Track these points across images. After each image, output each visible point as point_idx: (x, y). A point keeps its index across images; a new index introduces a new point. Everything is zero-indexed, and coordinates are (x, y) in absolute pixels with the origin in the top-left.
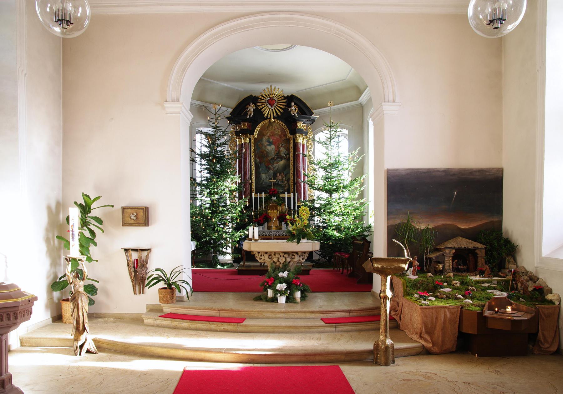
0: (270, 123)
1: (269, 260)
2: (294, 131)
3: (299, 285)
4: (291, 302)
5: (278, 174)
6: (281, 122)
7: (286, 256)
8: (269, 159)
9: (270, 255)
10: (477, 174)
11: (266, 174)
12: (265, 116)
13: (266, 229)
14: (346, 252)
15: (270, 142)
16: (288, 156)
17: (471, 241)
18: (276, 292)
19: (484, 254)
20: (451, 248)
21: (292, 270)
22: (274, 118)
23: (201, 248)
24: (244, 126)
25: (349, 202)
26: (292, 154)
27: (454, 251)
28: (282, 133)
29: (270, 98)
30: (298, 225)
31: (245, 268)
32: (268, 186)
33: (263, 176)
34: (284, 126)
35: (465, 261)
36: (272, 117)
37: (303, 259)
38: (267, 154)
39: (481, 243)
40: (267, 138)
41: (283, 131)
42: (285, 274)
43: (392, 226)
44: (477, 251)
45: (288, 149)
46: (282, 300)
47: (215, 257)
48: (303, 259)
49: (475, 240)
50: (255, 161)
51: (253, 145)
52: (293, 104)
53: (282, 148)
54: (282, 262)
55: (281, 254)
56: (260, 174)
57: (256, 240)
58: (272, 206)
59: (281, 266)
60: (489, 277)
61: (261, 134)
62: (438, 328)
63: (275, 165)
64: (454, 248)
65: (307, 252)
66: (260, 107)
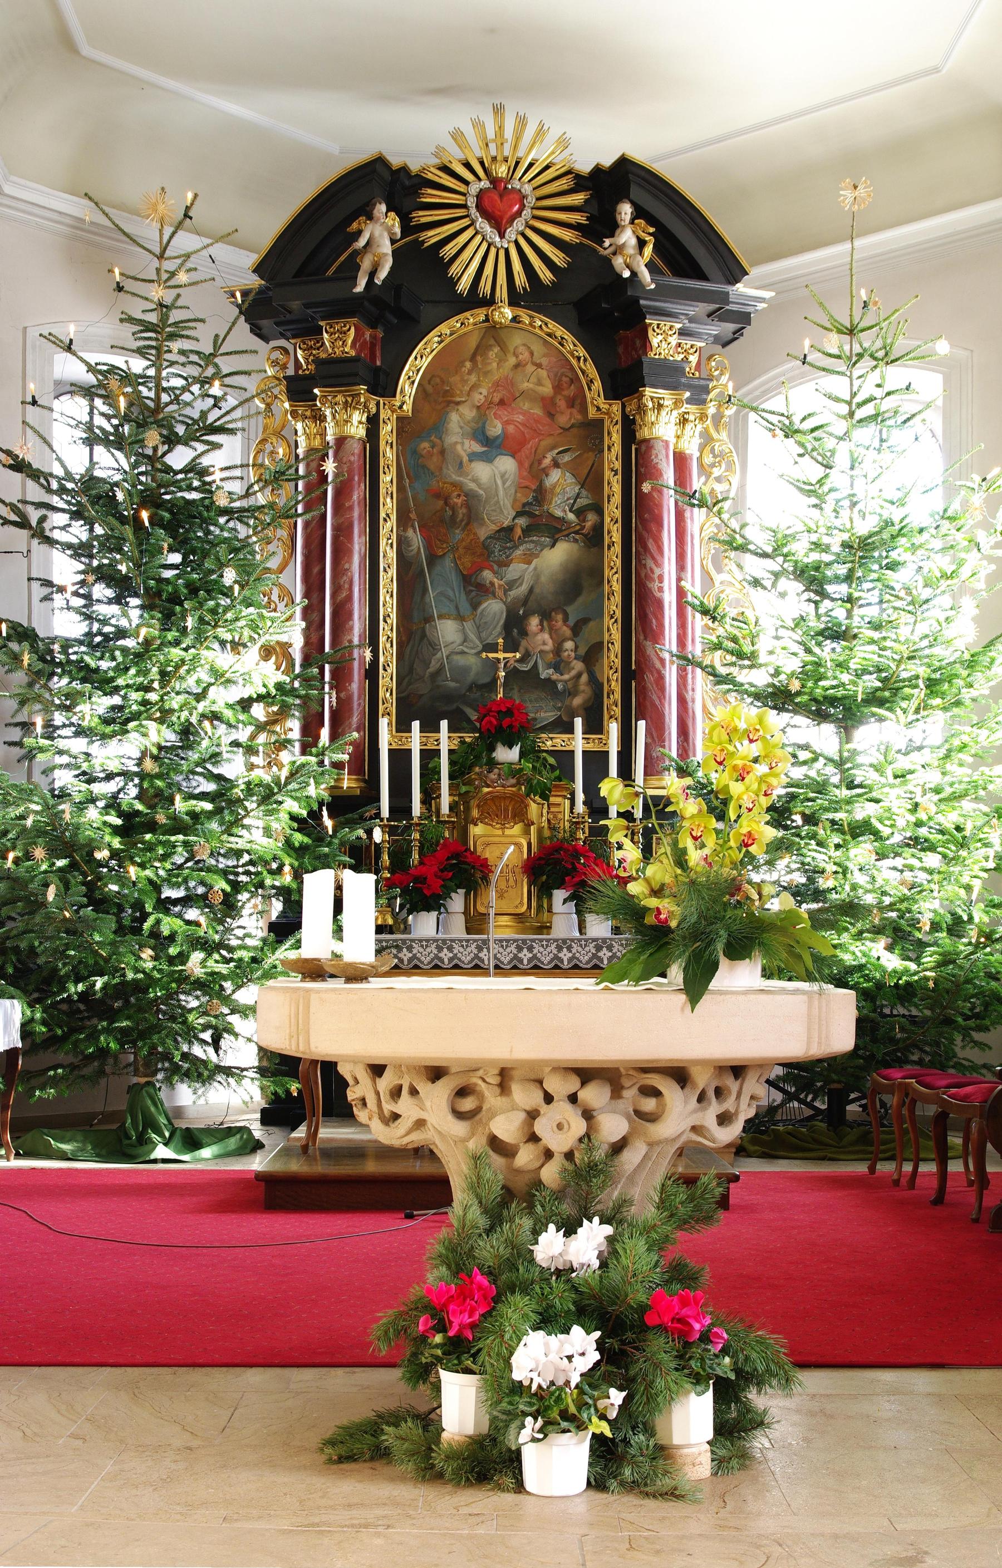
0: (492, 330)
1: (459, 1128)
2: (628, 376)
3: (706, 1337)
4: (638, 1487)
5: (534, 622)
6: (554, 327)
7: (594, 1095)
8: (483, 533)
9: (465, 1089)
11: (460, 618)
12: (464, 285)
13: (457, 928)
15: (487, 441)
16: (591, 518)
18: (510, 1399)
21: (645, 1210)
22: (515, 299)
23: (51, 1042)
24: (341, 340)
25: (960, 773)
26: (613, 509)
28: (558, 388)
29: (495, 181)
30: (694, 856)
31: (320, 1168)
32: (474, 686)
33: (448, 631)
34: (573, 347)
36: (502, 292)
37: (724, 1119)
38: (472, 507)
40: (468, 412)
41: (567, 379)
42: (585, 1246)
45: (592, 481)
46: (557, 1465)
47: (139, 1096)
48: (724, 1119)
50: (402, 544)
51: (388, 454)
52: (626, 210)
53: (555, 476)
54: (559, 1142)
55: (557, 1085)
56: (429, 619)
57: (356, 975)
58: (495, 798)
59: (551, 1174)
61: (436, 393)
63: (515, 569)
65: (762, 1065)
66: (432, 236)
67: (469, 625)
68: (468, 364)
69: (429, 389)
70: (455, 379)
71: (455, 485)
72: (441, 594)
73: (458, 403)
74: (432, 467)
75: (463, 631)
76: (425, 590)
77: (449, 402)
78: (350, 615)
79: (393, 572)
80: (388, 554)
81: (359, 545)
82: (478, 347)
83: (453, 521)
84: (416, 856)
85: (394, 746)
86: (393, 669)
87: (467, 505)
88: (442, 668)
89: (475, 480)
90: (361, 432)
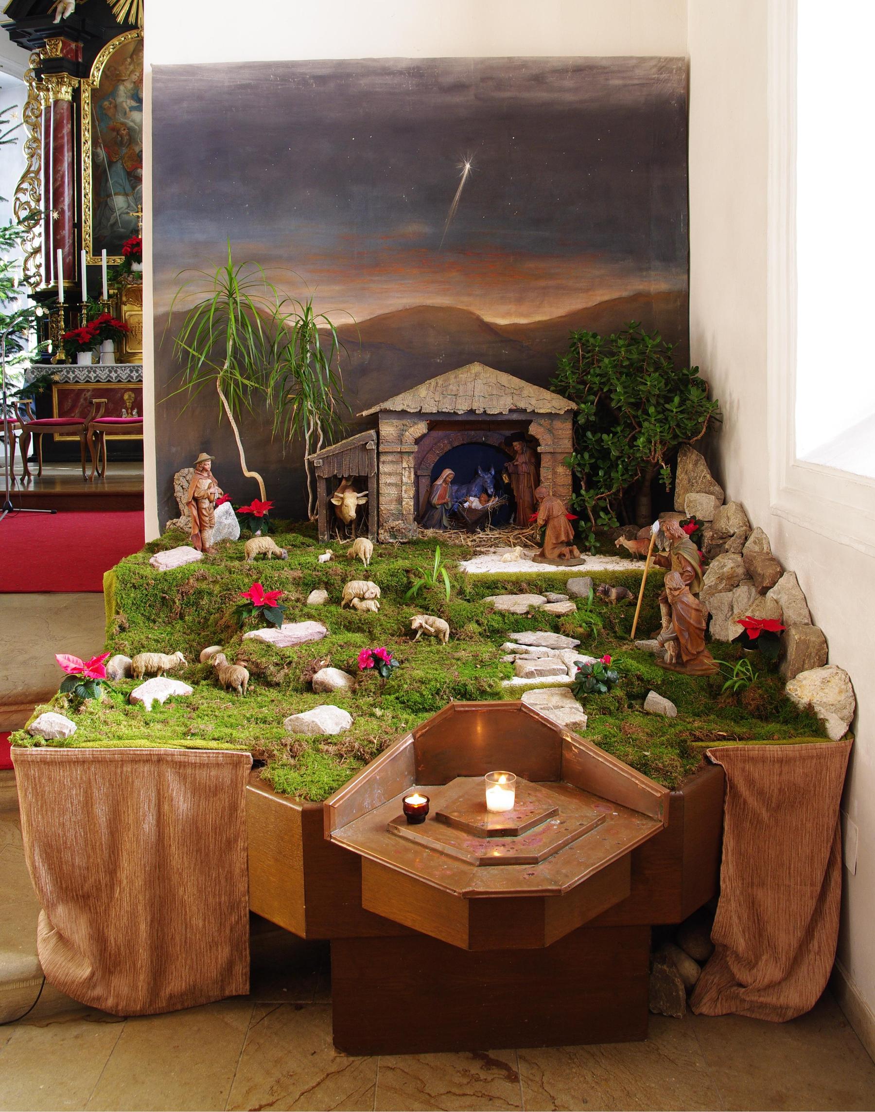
10: (568, 83)
11: (126, 195)
12: (120, 19)
14: (601, 440)
17: (516, 381)
19: (566, 444)
20: (404, 412)
27: (420, 428)
35: (481, 471)
39: (562, 391)
43: (180, 317)
44: (533, 430)
49: (540, 377)
50: (95, 155)
56: (109, 196)
60: (561, 559)
61: (112, 75)
62: (132, 870)
64: (420, 415)
67: (130, 198)
68: (129, 60)
69: (108, 73)
70: (122, 68)
71: (123, 124)
72: (116, 182)
73: (124, 81)
74: (110, 115)
75: (128, 201)
76: (107, 180)
77: (119, 80)
78: (63, 194)
79: (90, 171)
80: (87, 162)
81: (67, 157)
82: (134, 51)
83: (121, 144)
84: (84, 322)
85: (91, 264)
86: (90, 222)
87: (129, 134)
88: (116, 222)
89: (133, 121)
90: (69, 97)
